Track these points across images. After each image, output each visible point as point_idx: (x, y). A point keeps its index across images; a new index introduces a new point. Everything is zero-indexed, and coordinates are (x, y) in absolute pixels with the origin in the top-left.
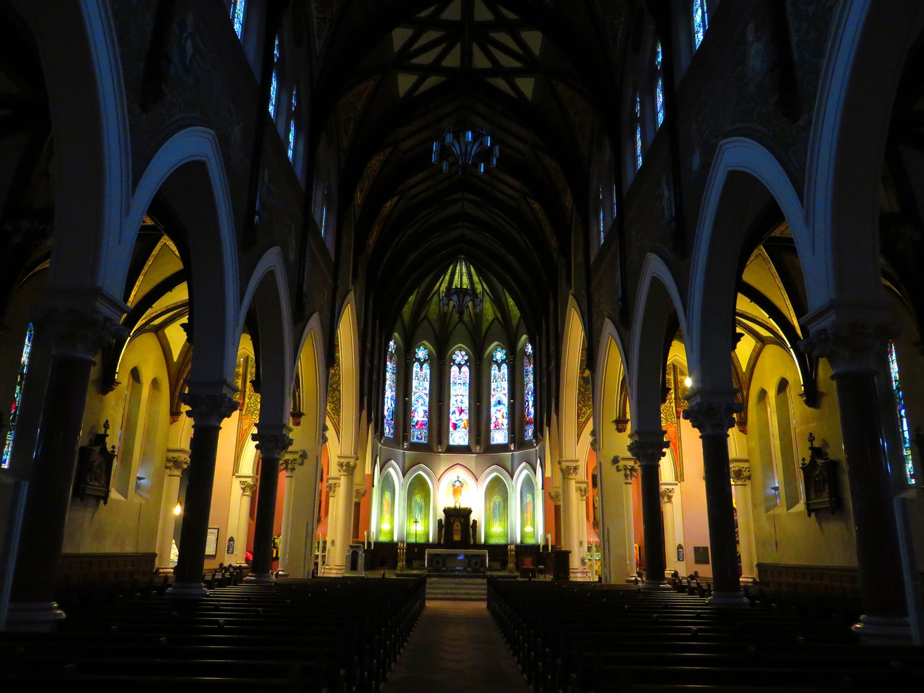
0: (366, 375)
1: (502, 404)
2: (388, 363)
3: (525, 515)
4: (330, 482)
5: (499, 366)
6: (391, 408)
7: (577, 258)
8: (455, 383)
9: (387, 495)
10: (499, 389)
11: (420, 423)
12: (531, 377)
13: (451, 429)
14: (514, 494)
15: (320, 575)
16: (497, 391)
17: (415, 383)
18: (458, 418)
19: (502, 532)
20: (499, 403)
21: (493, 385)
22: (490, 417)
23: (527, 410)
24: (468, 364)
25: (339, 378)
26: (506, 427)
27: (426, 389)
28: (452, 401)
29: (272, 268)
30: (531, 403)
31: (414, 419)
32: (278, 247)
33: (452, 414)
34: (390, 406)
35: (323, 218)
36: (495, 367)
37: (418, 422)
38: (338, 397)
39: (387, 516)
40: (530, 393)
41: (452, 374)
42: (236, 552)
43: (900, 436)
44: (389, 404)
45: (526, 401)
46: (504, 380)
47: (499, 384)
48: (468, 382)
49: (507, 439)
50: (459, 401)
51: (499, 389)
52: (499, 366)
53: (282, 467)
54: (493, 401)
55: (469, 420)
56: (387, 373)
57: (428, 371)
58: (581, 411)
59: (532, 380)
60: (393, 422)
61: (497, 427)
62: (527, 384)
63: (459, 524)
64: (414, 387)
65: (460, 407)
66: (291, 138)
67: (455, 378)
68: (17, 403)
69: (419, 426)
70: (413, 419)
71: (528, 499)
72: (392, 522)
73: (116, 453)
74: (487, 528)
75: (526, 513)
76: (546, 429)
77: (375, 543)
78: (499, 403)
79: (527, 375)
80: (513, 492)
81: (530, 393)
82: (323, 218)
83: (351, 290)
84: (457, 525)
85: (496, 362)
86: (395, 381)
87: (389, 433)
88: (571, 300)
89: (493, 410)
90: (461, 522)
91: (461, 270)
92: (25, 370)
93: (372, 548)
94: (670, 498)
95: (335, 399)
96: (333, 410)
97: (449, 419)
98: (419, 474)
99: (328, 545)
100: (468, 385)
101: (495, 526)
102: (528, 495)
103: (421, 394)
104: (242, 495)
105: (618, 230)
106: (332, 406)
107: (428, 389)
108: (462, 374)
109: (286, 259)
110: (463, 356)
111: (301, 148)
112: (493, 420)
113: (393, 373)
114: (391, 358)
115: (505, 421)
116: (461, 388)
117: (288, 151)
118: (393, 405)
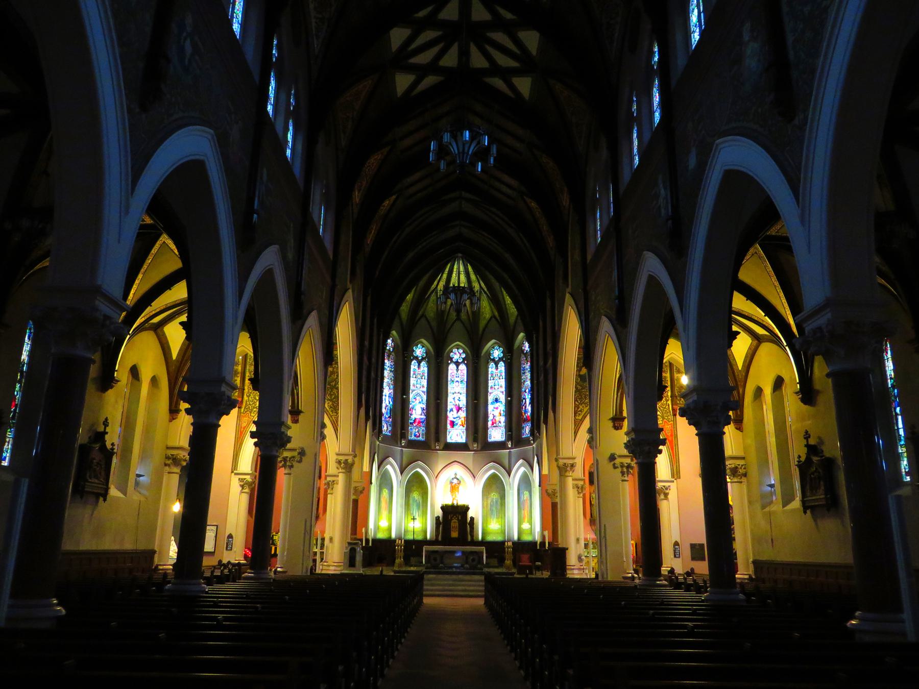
0: (364, 373)
1: (500, 402)
2: (386, 361)
3: (523, 512)
4: (329, 479)
5: (497, 364)
6: (389, 405)
7: (574, 256)
8: (453, 381)
9: (385, 492)
10: (496, 387)
11: (417, 421)
12: (528, 375)
13: (449, 426)
14: (511, 491)
15: (318, 571)
16: (495, 389)
17: (413, 381)
18: (455, 415)
19: (499, 529)
20: (497, 400)
21: (491, 383)
22: (488, 414)
23: (524, 407)
24: (466, 362)
25: (338, 376)
26: (503, 424)
27: (423, 387)
28: (450, 399)
29: (271, 267)
30: (528, 401)
31: (412, 417)
32: (276, 246)
33: (450, 411)
34: (388, 404)
35: (321, 217)
36: (492, 365)
37: (415, 419)
38: (337, 394)
39: (384, 513)
40: (527, 391)
41: (450, 372)
42: (234, 549)
43: (895, 433)
44: (387, 401)
45: (523, 399)
46: (501, 377)
47: (497, 381)
48: (465, 380)
49: (504, 436)
50: (456, 399)
51: (496, 387)
52: (497, 364)
53: (281, 465)
54: (491, 398)
55: (467, 418)
56: (385, 371)
57: (426, 369)
58: (578, 408)
59: (529, 378)
60: (391, 420)
61: (495, 425)
62: (524, 381)
63: (456, 521)
64: (411, 384)
65: (458, 404)
66: (290, 137)
67: (453, 376)
68: (17, 401)
69: (416, 424)
70: (410, 417)
71: (525, 496)
72: (390, 519)
73: (115, 451)
74: (485, 525)
75: (524, 510)
76: (543, 427)
77: (373, 540)
78: (497, 400)
79: (524, 373)
80: (510, 489)
81: (527, 391)
82: (321, 217)
83: (349, 289)
84: (455, 522)
85: (493, 360)
86: (393, 379)
87: (387, 430)
88: (568, 298)
89: (490, 407)
90: (458, 519)
91: (459, 268)
92: (25, 368)
93: (370, 544)
94: (666, 495)
95: (333, 396)
96: (331, 407)
97: (446, 417)
98: (417, 471)
99: (327, 542)
100: (465, 383)
101: (492, 523)
102: (525, 492)
103: (419, 392)
104: (241, 492)
105: (615, 228)
106: (331, 403)
107: (426, 386)
108: (459, 372)
109: (284, 258)
110: (460, 354)
111: (299, 147)
112: (491, 418)
113: (391, 371)
114: (389, 356)
115: (503, 419)
116: (458, 386)
117: (286, 150)
118: (391, 403)
